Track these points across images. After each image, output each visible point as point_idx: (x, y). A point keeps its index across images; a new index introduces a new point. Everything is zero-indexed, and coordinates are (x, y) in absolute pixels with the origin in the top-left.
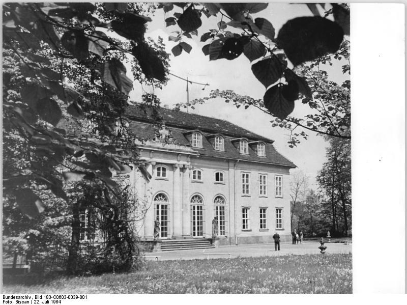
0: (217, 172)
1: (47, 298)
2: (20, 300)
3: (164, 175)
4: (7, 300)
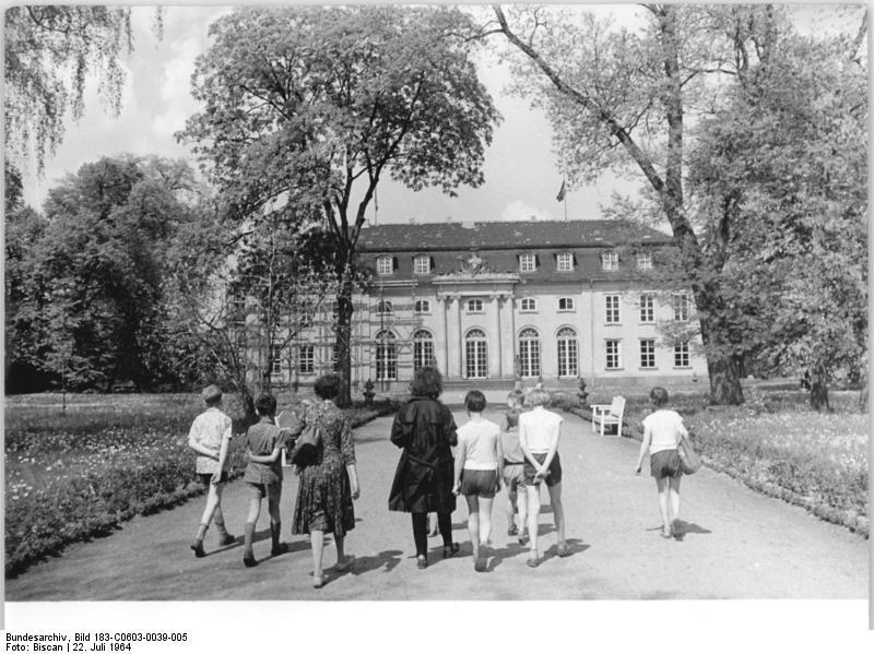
0: (562, 298)
1: (102, 638)
2: (43, 643)
3: (479, 308)
4: (15, 643)
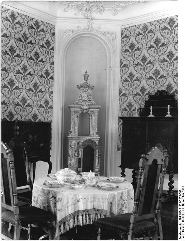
2: (182, 230)
4: (182, 237)
